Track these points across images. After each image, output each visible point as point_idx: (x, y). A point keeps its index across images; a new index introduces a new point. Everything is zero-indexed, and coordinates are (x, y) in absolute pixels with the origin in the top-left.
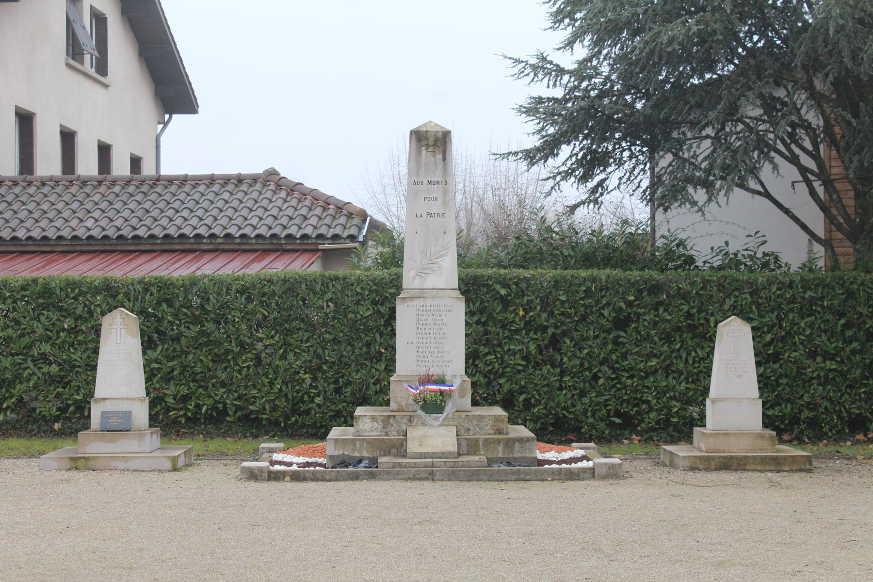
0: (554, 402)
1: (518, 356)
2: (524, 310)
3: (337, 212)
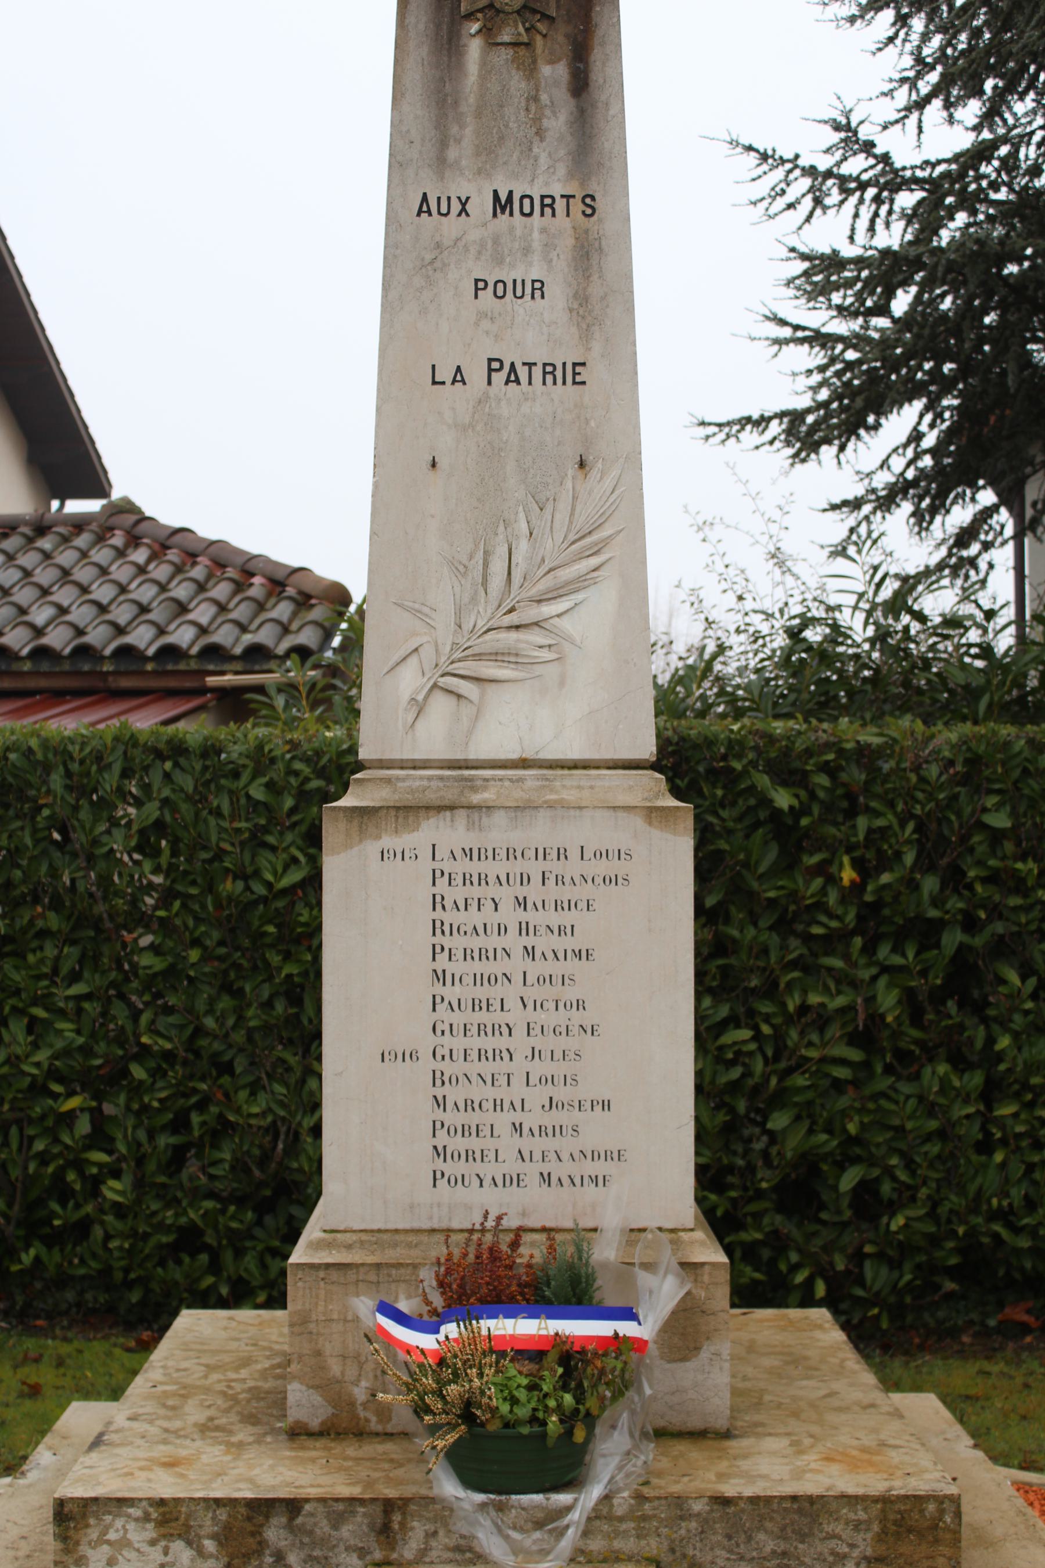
0: (962, 1190)
1: (834, 1031)
2: (858, 864)
3: (269, 595)
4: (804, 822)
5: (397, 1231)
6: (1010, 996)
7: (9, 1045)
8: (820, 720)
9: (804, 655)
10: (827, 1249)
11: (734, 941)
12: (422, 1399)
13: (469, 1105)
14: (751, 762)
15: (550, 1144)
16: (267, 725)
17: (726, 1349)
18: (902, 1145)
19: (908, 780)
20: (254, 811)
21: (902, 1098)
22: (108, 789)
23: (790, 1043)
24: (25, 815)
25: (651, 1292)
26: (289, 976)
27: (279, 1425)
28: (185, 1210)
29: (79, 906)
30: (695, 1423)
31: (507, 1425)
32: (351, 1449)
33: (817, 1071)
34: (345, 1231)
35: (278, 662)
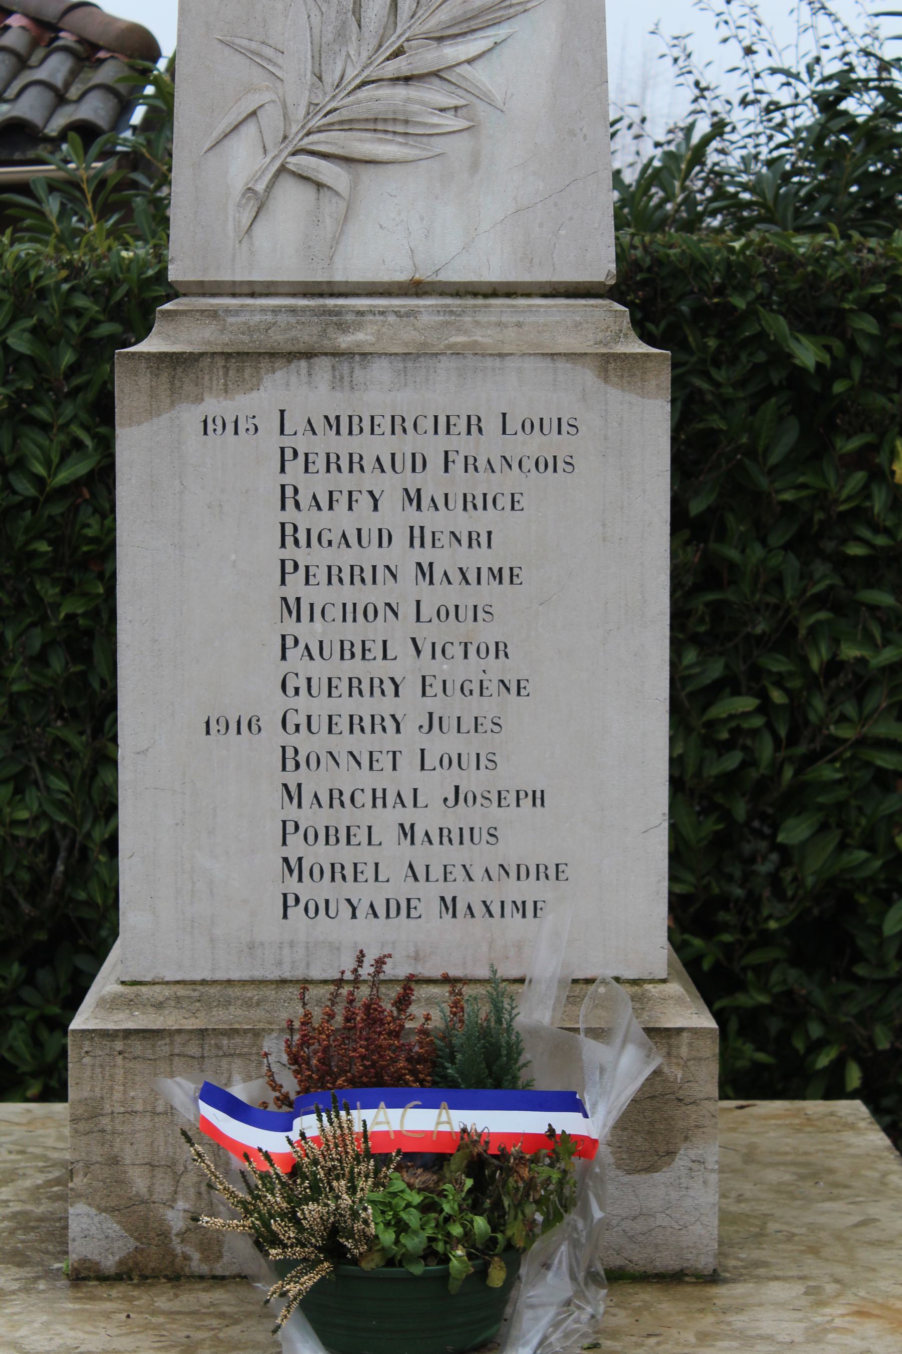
1: (878, 699)
3: (34, 44)
4: (839, 387)
5: (229, 982)
8: (865, 235)
9: (844, 137)
10: (865, 1018)
11: (732, 566)
12: (267, 1225)
13: (335, 798)
14: (760, 296)
15: (455, 854)
16: (32, 240)
17: (712, 1154)
20: (15, 370)
23: (812, 717)
25: (602, 1070)
26: (71, 617)
27: (57, 1265)
30: (667, 1261)
31: (390, 1262)
32: (163, 1299)
33: (854, 757)
34: (154, 983)
35: (49, 147)
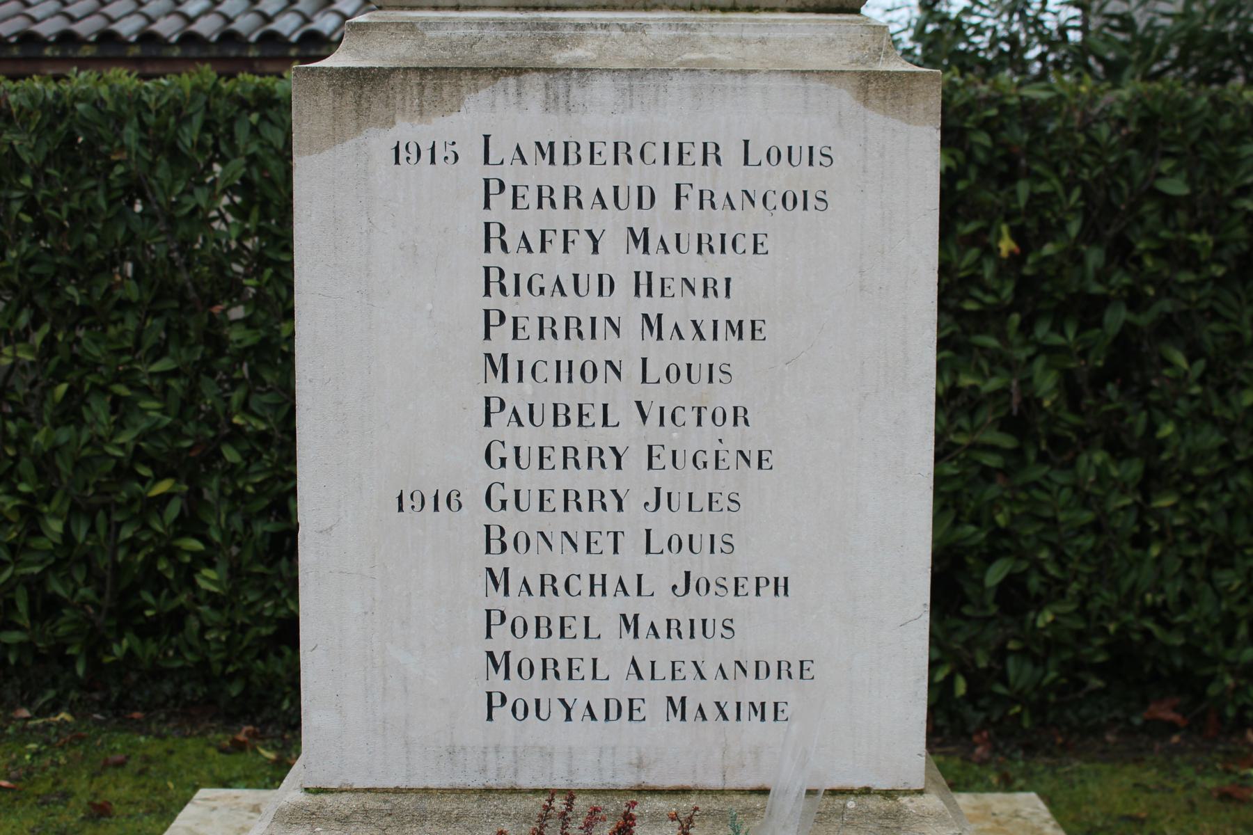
1: (986, 415)
2: (1017, 235)
6: (1176, 380)
7: (91, 425)
10: (969, 645)
13: (548, 584)
15: (684, 649)
18: (1053, 538)
19: (1075, 140)
21: (1055, 488)
22: (188, 143)
24: (99, 173)
28: (284, 600)
29: (160, 274)
